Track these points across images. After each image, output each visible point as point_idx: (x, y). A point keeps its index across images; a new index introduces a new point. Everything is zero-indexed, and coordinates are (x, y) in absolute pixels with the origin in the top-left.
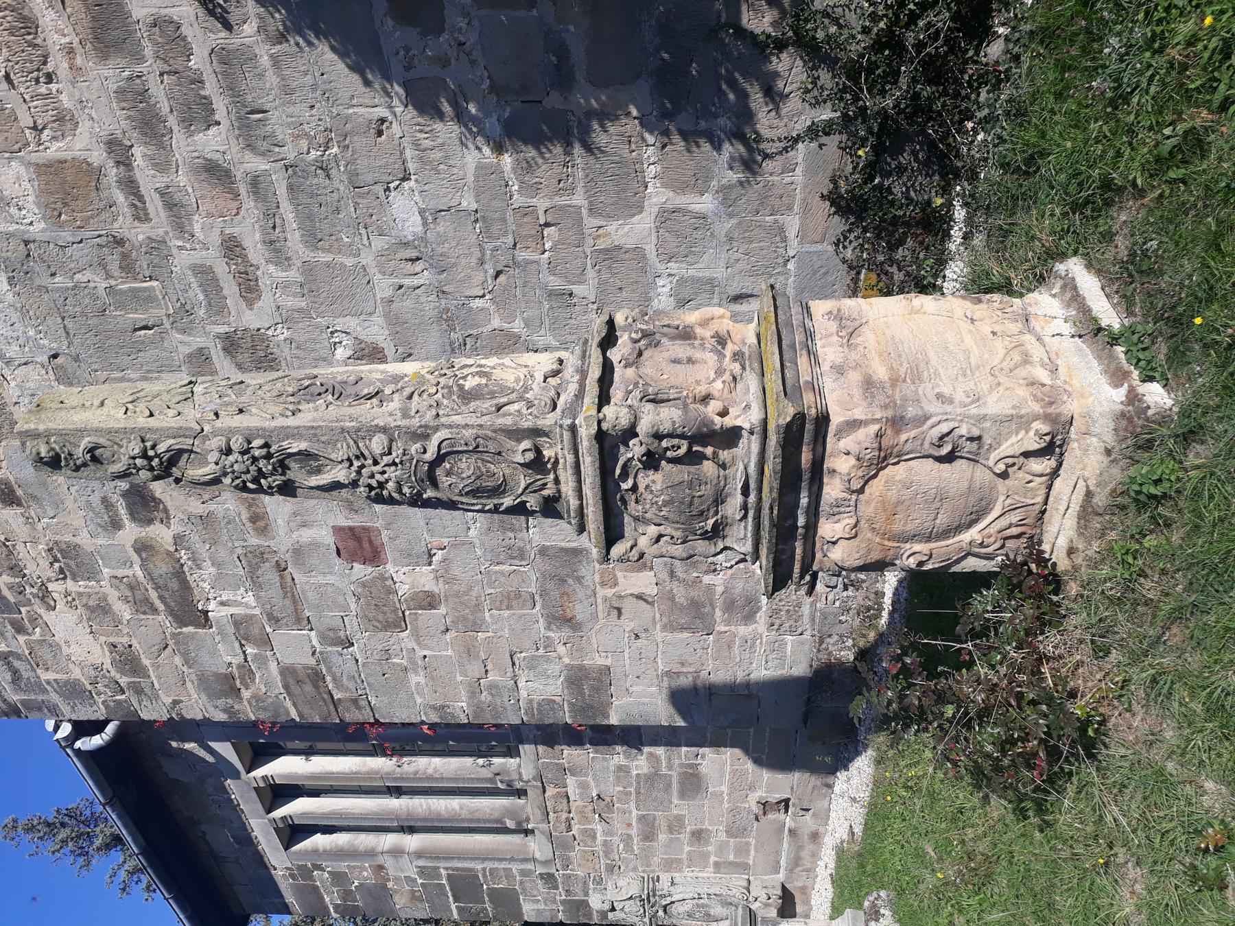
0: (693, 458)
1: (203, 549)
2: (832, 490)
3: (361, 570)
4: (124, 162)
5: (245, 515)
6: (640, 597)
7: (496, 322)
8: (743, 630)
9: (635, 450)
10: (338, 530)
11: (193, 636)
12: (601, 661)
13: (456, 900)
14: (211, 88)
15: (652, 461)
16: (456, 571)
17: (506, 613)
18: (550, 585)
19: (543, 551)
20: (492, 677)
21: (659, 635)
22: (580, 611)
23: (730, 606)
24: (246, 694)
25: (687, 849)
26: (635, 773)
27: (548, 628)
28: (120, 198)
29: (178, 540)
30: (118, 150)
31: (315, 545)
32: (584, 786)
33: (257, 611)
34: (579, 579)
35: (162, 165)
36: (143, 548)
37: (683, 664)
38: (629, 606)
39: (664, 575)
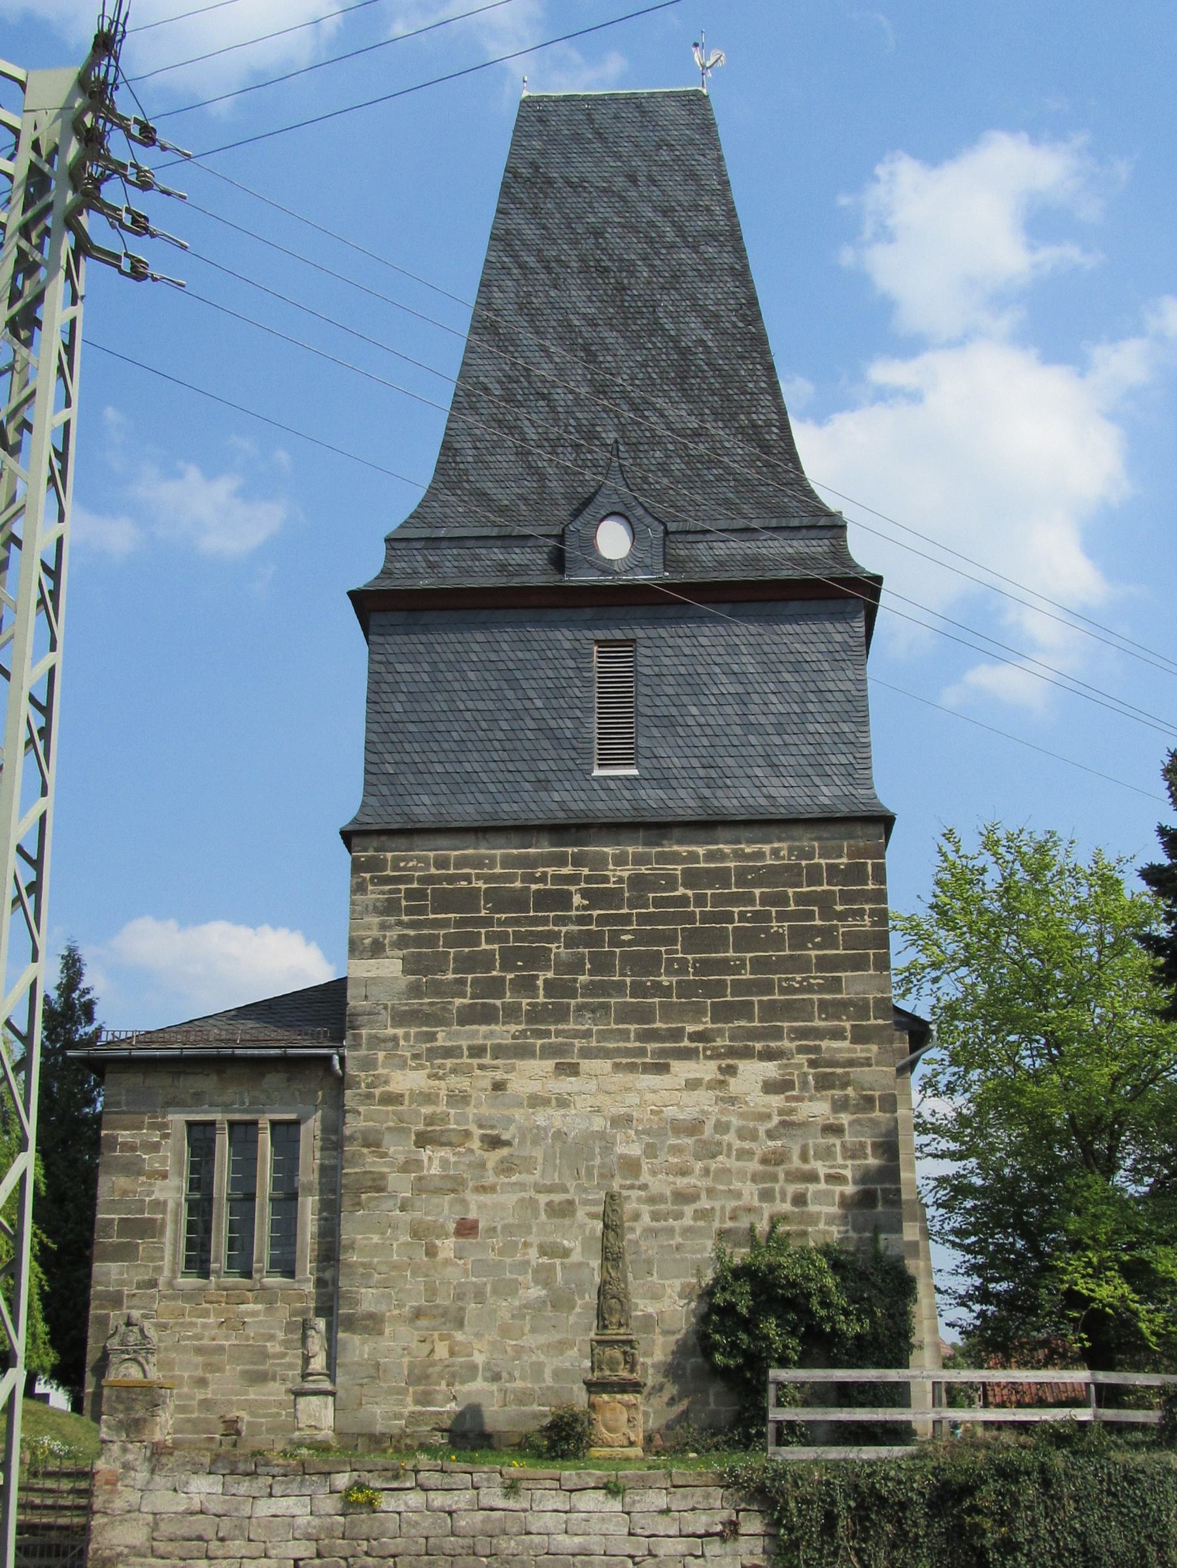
0: (626, 1362)
1: (466, 1160)
2: (619, 1396)
3: (452, 1227)
4: (640, 1188)
5: (486, 1184)
6: (432, 1351)
7: (579, 1302)
8: (409, 1399)
9: (628, 1349)
10: (476, 1222)
11: (410, 1137)
12: (387, 1331)
13: (121, 1219)
14: (663, 1223)
15: (625, 1353)
16: (450, 1269)
17: (422, 1288)
18: (441, 1311)
19: (462, 1309)
20: (376, 1275)
21: (406, 1360)
22: (423, 1322)
23: (426, 1394)
24: (365, 1150)
25: (186, 1375)
26: (268, 1344)
27: (411, 1307)
28: (628, 1182)
29: (472, 1151)
30: (644, 1187)
31: (467, 1210)
32: (254, 1314)
33: (425, 1172)
34: (445, 1323)
35: (639, 1199)
36: (467, 1134)
37: (385, 1371)
38: (426, 1347)
39: (446, 1363)
